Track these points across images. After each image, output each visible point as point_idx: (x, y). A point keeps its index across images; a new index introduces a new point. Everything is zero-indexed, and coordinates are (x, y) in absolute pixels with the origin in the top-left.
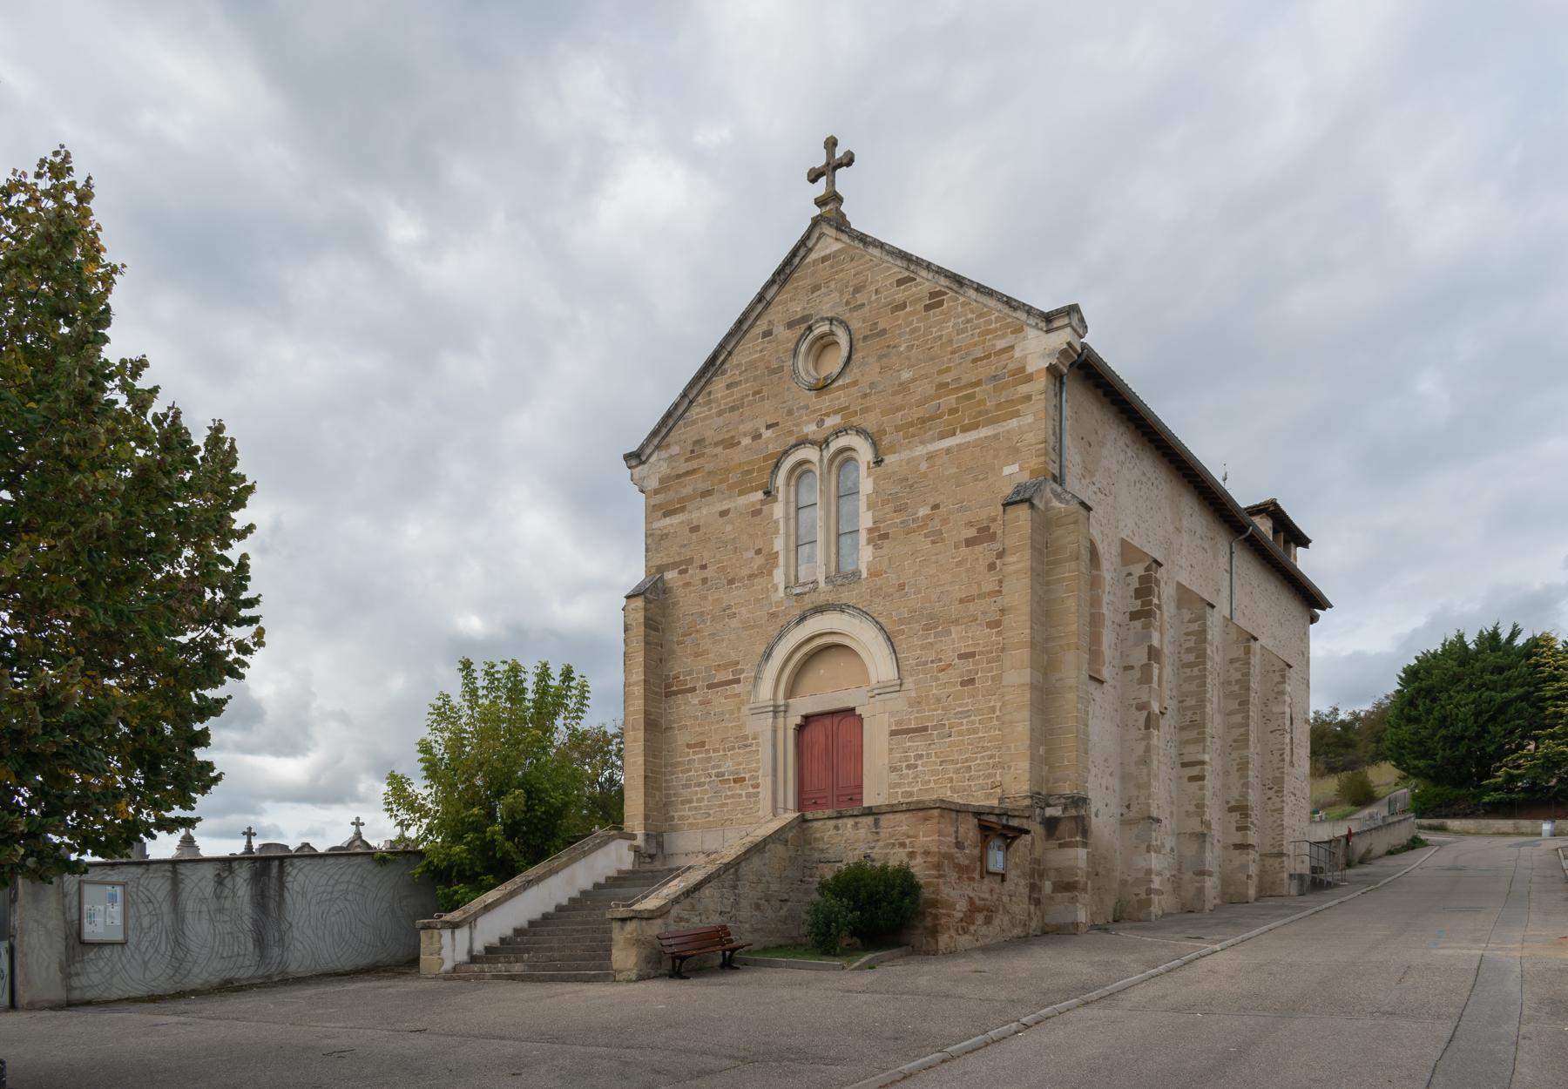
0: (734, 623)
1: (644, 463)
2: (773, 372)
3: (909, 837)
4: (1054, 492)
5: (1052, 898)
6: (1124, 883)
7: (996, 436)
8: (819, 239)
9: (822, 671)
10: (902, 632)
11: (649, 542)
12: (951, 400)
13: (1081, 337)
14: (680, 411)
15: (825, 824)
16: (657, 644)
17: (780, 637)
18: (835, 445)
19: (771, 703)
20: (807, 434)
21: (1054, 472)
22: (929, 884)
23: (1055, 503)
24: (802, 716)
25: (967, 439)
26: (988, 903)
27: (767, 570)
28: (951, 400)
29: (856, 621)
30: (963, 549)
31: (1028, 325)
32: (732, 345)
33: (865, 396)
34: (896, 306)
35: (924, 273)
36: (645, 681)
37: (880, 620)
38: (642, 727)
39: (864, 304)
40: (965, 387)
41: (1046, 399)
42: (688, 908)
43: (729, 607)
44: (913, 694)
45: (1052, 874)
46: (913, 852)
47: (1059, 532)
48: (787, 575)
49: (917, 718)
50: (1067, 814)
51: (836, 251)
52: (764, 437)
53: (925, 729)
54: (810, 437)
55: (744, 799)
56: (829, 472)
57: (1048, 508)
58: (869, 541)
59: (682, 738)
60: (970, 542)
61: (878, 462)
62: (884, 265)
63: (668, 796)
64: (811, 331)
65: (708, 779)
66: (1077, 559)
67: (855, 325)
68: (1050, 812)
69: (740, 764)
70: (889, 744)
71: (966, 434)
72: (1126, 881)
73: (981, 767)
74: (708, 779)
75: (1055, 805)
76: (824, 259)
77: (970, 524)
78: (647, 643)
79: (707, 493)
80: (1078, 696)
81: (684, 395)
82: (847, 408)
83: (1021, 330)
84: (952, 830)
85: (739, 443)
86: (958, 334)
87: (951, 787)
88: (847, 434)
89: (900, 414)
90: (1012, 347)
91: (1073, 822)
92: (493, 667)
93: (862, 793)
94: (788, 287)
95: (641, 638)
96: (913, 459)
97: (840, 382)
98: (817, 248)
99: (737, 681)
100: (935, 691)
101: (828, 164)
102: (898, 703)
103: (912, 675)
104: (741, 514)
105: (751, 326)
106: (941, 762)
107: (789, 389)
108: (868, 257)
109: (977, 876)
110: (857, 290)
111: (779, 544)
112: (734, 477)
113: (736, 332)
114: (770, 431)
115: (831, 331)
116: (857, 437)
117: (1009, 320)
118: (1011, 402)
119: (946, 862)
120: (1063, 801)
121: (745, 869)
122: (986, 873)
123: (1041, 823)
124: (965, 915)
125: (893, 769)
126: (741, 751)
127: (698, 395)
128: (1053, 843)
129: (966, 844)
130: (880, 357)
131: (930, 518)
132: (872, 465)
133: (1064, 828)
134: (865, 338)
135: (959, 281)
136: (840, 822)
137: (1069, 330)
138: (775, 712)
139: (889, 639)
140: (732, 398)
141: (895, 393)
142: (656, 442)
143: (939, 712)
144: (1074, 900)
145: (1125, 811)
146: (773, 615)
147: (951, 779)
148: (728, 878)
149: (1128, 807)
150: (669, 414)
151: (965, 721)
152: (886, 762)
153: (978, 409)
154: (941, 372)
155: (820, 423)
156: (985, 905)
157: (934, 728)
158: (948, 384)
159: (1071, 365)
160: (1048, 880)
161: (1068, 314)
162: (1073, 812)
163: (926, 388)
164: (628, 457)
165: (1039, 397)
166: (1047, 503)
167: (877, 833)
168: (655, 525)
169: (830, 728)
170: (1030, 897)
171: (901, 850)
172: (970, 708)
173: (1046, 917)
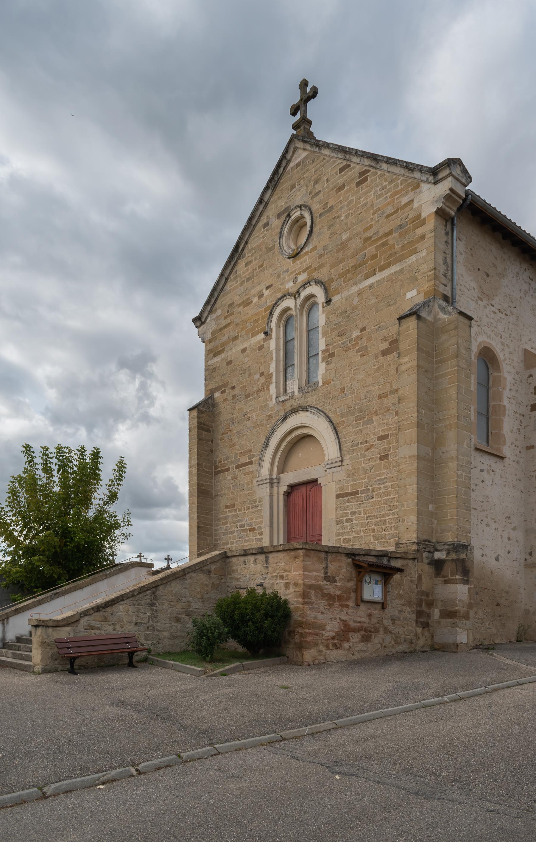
0: (249, 424)
1: (203, 323)
2: (270, 250)
3: (286, 571)
4: (440, 306)
5: (439, 623)
6: (527, 612)
7: (401, 271)
8: (294, 152)
9: (300, 454)
10: (343, 423)
11: (207, 374)
12: (372, 250)
13: (466, 186)
14: (221, 286)
15: (238, 560)
16: (208, 440)
17: (273, 432)
18: (303, 295)
19: (268, 477)
20: (288, 289)
21: (445, 293)
22: (297, 609)
23: (442, 316)
24: (288, 486)
25: (383, 276)
26: (365, 625)
27: (265, 387)
28: (372, 250)
29: (316, 417)
30: (381, 359)
31: (423, 181)
32: (247, 236)
33: (321, 256)
34: (339, 188)
35: (354, 159)
36: (198, 464)
37: (330, 415)
38: (197, 495)
39: (320, 191)
40: (381, 237)
41: (435, 236)
42: (100, 619)
43: (247, 413)
44: (350, 468)
45: (440, 604)
46: (288, 583)
47: (444, 337)
48: (277, 388)
49: (352, 485)
50: (450, 558)
51: (304, 158)
52: (265, 295)
53: (357, 493)
54: (290, 291)
55: (254, 542)
56: (302, 314)
57: (436, 319)
58: (324, 359)
59: (223, 501)
60: (385, 353)
61: (328, 302)
62: (332, 160)
63: (216, 540)
64: (290, 217)
65: (236, 529)
66: (457, 356)
67: (315, 207)
68: (438, 555)
69: (252, 519)
70: (336, 504)
71: (382, 273)
72: (529, 611)
73: (392, 521)
74: (236, 529)
75: (441, 550)
76: (297, 165)
77: (385, 339)
78: (199, 439)
79: (235, 338)
80: (458, 464)
81: (222, 275)
82: (310, 267)
83: (418, 186)
84: (321, 566)
85: (252, 301)
86: (377, 199)
87: (373, 536)
88: (310, 285)
89: (341, 265)
90: (412, 201)
91: (454, 564)
92: (47, 450)
93: (321, 540)
94: (278, 190)
95: (196, 436)
96: (349, 296)
97: (306, 249)
98: (293, 158)
99: (251, 463)
100: (363, 465)
101: (301, 99)
102: (340, 474)
103: (349, 454)
104: (253, 350)
105: (258, 221)
106: (368, 517)
107: (278, 260)
108: (322, 157)
109: (351, 603)
110: (316, 182)
111: (273, 368)
112: (249, 326)
113: (249, 226)
114: (268, 291)
115: (301, 214)
116: (316, 286)
117: (410, 181)
118: (411, 243)
119: (313, 592)
120: (446, 547)
121: (162, 591)
122: (360, 601)
123: (429, 564)
124: (338, 635)
125: (338, 522)
126: (253, 510)
127: (230, 273)
128: (439, 580)
129: (337, 578)
130: (330, 227)
131: (360, 338)
132: (325, 305)
133: (448, 568)
134: (321, 215)
135: (374, 158)
136: (246, 558)
137: (450, 178)
138: (271, 484)
139: (335, 428)
140: (248, 273)
141: (338, 251)
142: (209, 308)
143: (366, 480)
144: (454, 625)
145: (528, 557)
146: (270, 417)
147: (374, 530)
148: (145, 598)
149: (530, 554)
150: (214, 289)
151: (382, 486)
152: (334, 517)
153: (390, 252)
154: (366, 230)
155: (295, 280)
156: (362, 627)
157: (363, 492)
158: (371, 237)
159: (459, 210)
160: (437, 608)
161: (448, 166)
162: (454, 556)
163: (357, 243)
164: (195, 320)
165: (430, 235)
166: (435, 317)
167: (267, 567)
168: (210, 363)
169: (305, 495)
170: (417, 621)
171: (281, 581)
172: (385, 476)
173: (435, 637)
